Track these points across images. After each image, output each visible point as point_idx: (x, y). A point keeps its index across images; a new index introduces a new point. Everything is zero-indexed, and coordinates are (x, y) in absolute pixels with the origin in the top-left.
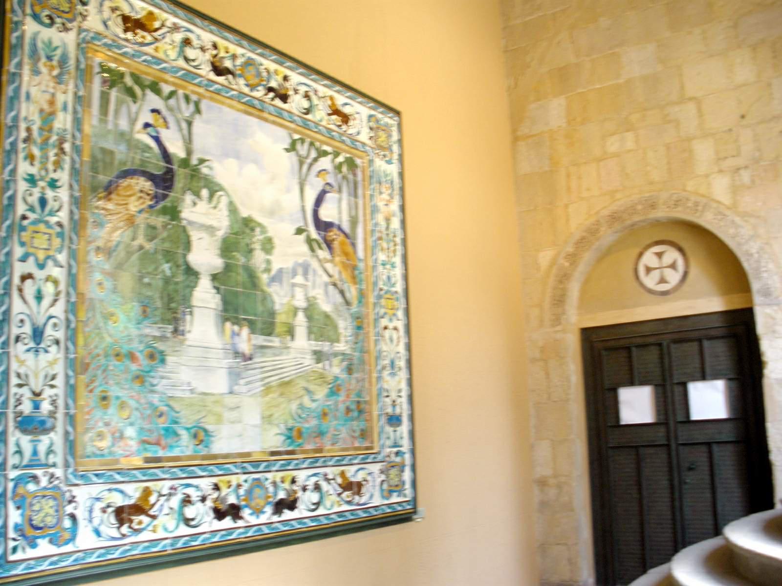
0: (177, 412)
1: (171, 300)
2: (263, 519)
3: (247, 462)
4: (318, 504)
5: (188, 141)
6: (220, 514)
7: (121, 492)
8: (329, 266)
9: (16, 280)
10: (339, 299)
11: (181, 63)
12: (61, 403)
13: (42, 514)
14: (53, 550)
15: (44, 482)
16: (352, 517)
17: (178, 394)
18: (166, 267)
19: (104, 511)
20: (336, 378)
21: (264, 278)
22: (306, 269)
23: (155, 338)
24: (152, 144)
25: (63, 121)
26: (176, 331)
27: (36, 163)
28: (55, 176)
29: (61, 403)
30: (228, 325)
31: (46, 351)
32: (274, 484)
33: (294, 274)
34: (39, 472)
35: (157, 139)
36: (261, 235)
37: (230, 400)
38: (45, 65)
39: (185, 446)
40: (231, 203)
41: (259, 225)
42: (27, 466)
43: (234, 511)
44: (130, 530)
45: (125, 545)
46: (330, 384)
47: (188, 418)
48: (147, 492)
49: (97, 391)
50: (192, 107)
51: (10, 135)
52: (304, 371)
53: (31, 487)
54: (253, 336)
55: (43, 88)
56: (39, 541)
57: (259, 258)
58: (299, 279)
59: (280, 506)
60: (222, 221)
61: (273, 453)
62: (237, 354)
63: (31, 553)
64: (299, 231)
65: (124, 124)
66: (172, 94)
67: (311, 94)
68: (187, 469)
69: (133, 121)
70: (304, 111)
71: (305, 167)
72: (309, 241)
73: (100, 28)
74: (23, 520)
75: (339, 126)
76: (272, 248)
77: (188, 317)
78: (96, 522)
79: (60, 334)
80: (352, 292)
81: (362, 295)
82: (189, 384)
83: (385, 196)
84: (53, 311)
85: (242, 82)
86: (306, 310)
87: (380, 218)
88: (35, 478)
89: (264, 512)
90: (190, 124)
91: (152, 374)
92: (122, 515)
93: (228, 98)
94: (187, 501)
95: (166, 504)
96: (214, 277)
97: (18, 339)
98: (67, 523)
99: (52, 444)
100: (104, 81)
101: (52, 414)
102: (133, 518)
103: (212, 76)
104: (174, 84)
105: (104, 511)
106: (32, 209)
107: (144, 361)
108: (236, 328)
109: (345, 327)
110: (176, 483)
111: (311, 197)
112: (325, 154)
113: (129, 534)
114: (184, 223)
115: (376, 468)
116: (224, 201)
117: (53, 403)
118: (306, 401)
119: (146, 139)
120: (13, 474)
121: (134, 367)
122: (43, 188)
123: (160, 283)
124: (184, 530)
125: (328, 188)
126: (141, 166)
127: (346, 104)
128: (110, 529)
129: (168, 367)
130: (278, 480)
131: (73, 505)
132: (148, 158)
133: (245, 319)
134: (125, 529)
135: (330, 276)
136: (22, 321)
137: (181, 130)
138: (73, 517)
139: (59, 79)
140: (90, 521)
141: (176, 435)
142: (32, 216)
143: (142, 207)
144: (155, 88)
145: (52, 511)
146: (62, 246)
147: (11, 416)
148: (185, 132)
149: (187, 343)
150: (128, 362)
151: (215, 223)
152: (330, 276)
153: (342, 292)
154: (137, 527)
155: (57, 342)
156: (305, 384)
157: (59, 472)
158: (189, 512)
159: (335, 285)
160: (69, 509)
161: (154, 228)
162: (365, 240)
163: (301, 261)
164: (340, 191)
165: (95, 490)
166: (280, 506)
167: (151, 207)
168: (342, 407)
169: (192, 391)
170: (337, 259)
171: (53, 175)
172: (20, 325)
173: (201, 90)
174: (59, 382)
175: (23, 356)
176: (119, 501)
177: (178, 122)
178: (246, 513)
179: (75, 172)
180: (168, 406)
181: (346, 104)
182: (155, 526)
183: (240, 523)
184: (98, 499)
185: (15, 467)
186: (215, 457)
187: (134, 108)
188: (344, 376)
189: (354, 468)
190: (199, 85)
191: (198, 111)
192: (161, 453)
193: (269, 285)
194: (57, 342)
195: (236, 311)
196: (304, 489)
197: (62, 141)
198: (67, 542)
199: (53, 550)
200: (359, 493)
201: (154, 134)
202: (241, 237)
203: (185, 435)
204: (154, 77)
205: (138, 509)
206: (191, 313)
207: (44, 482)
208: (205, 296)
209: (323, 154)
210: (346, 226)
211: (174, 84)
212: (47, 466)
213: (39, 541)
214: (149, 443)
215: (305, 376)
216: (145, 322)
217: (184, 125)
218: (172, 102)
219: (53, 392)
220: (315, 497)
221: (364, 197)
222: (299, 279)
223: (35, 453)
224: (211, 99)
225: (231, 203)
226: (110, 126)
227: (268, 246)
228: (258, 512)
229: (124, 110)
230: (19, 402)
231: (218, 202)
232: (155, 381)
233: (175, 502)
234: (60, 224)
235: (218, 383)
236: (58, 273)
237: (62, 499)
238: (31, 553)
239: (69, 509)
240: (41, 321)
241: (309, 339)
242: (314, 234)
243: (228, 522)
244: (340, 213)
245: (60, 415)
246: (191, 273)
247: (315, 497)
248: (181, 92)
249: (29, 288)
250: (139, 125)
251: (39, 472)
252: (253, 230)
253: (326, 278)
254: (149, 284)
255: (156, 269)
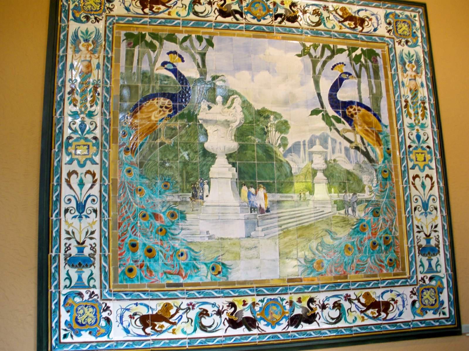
0: (196, 253)
1: (189, 175)
2: (279, 329)
3: (260, 288)
4: (338, 319)
5: (202, 66)
6: (234, 324)
7: (147, 306)
8: (350, 136)
9: (64, 176)
10: (362, 158)
11: (192, 16)
12: (98, 248)
13: (85, 316)
14: (92, 338)
15: (86, 297)
16: (377, 330)
17: (197, 239)
18: (185, 154)
19: (131, 317)
20: (360, 220)
21: (281, 151)
22: (324, 141)
23: (175, 203)
24: (170, 74)
25: (97, 75)
26: (194, 196)
27: (78, 104)
28: (93, 109)
29: (98, 248)
30: (245, 189)
31: (87, 217)
32: (291, 303)
33: (312, 143)
34: (83, 291)
35: (175, 71)
36: (275, 120)
37: (249, 243)
38: (83, 45)
39: (204, 275)
40: (244, 102)
41: (274, 113)
42: (74, 287)
43: (250, 323)
44: (153, 331)
45: (149, 340)
46: (353, 225)
47: (207, 256)
48: (167, 307)
49: (128, 241)
50: (204, 43)
51: (60, 91)
52: (325, 217)
53: (78, 299)
54: (268, 195)
55: (83, 59)
56: (82, 332)
57: (274, 137)
58: (317, 148)
59: (295, 321)
60: (236, 115)
61: (290, 280)
62: (253, 208)
63: (76, 339)
64: (315, 112)
65: (145, 67)
66: (185, 39)
67: (321, 10)
68: (203, 291)
69: (152, 64)
70: (71, 113)
71: (319, 65)
72: (326, 118)
73: (124, 12)
74: (71, 319)
75: (353, 29)
76: (288, 128)
77: (206, 187)
78: (125, 324)
79: (97, 206)
80: (377, 152)
81: (388, 153)
82: (208, 232)
83: (410, 73)
84: (92, 192)
85: (249, 17)
86: (324, 171)
87: (405, 91)
88: (80, 295)
89: (280, 324)
90: (203, 55)
91: (173, 227)
92: (146, 321)
93: (238, 30)
94: (204, 313)
95: (184, 316)
96: (229, 156)
97: (66, 211)
98: (103, 323)
99: (92, 274)
100: (129, 44)
101: (92, 256)
102: (156, 323)
103: (220, 19)
104: (186, 32)
105: (131, 317)
106: (75, 131)
107: (166, 219)
108: (253, 190)
109: (369, 180)
110: (193, 301)
111: (325, 86)
112: (341, 51)
113: (152, 333)
114: (201, 122)
115: (407, 291)
116: (238, 101)
117: (92, 248)
118: (328, 240)
119: (164, 72)
120: (64, 291)
121: (158, 224)
122: (83, 118)
123: (180, 166)
124: (200, 333)
125: (344, 76)
126: (162, 90)
127: (359, 11)
128: (137, 329)
129: (188, 223)
130: (295, 300)
131: (108, 312)
132: (167, 84)
133: (260, 183)
134: (148, 330)
135: (350, 142)
136: (69, 200)
137: (194, 59)
138: (108, 320)
139: (93, 52)
140: (122, 323)
141: (196, 268)
142: (75, 136)
143: (163, 117)
144: (171, 38)
145: (92, 315)
146: (98, 151)
147: (62, 257)
148: (200, 61)
149: (205, 204)
150: (153, 221)
151: (230, 118)
152: (350, 142)
153: (366, 154)
154: (159, 329)
155: (95, 211)
156: (325, 227)
157: (97, 291)
158: (206, 321)
159: (357, 148)
160: (105, 314)
161: (174, 129)
162: (390, 110)
163: (318, 134)
164: (359, 76)
165: (125, 304)
166: (295, 321)
167: (170, 116)
168: (367, 243)
169: (210, 237)
170: (358, 128)
171: (89, 109)
172: (68, 202)
173: (212, 30)
174: (97, 235)
175: (70, 221)
176: (144, 311)
177: (193, 56)
178: (262, 324)
179: (106, 104)
180: (188, 248)
181: (359, 11)
182: (174, 330)
183: (255, 331)
184: (128, 310)
185: (66, 287)
186: (233, 283)
187: (153, 55)
188: (370, 217)
189: (379, 292)
190: (209, 27)
191: (210, 43)
192: (182, 281)
193: (285, 156)
194: (95, 211)
195: (253, 177)
196: (324, 307)
197: (95, 88)
198: (103, 335)
199: (92, 338)
200: (386, 311)
201: (172, 67)
202: (255, 125)
203: (204, 269)
204: (169, 31)
205: (161, 317)
206: (209, 184)
207: (86, 297)
208: (222, 171)
209: (334, 52)
210: (366, 101)
211: (186, 32)
212: (89, 287)
213: (82, 332)
214: (170, 273)
215: (328, 221)
216: (167, 193)
217: (198, 57)
218: (187, 43)
219: (92, 242)
220: (335, 313)
221: (386, 76)
222: (317, 148)
223: (80, 278)
224: (221, 34)
225: (244, 102)
226: (134, 70)
227: (283, 127)
228: (274, 323)
229: (146, 57)
230: (68, 248)
231: (232, 103)
232: (176, 232)
233: (193, 314)
234: (95, 138)
235: (236, 230)
236: (96, 169)
237: (99, 307)
238: (76, 339)
239: (105, 314)
240: (82, 199)
241: (330, 192)
242: (331, 112)
243: (242, 330)
244: (359, 92)
245: (97, 256)
246: (209, 157)
247: (335, 313)
248: (193, 36)
249: (418, 182)
250: (158, 64)
251: (83, 291)
252: (268, 117)
253: (348, 145)
254: (171, 167)
255: (177, 156)
